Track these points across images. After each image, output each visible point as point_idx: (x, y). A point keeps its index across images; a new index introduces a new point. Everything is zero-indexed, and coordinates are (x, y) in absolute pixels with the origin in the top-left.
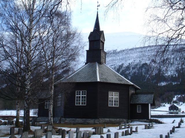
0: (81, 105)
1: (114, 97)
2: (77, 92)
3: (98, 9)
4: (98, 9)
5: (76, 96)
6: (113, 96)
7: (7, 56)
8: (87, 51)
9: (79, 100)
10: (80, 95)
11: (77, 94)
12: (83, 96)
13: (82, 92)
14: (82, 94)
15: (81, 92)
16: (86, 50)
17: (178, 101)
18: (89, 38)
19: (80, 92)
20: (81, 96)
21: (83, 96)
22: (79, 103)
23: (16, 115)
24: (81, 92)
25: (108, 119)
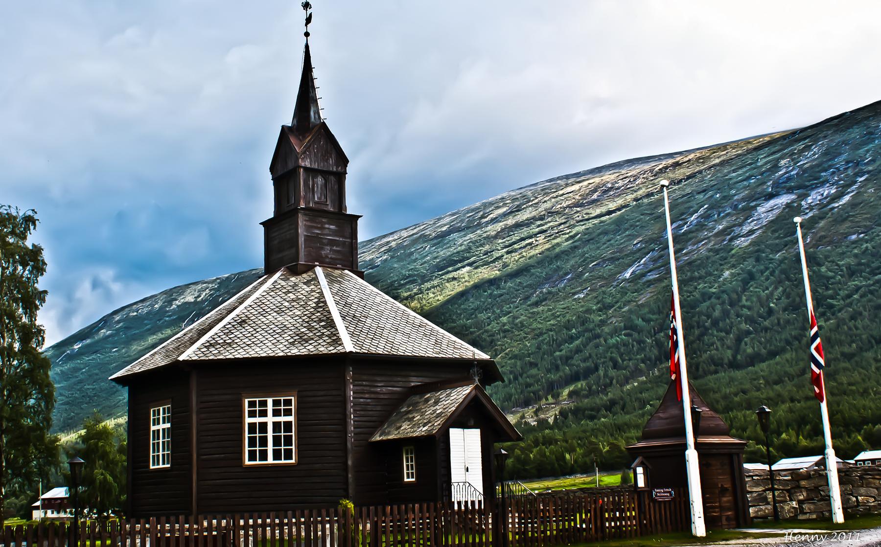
0: (270, 460)
1: (269, 423)
2: (252, 404)
3: (307, 34)
4: (307, 34)
5: (248, 420)
6: (274, 415)
7: (834, 289)
8: (266, 224)
9: (264, 442)
10: (266, 416)
11: (252, 414)
12: (277, 419)
13: (276, 403)
14: (276, 413)
15: (270, 401)
16: (357, 217)
17: (865, 433)
18: (272, 169)
19: (264, 404)
20: (270, 419)
21: (277, 419)
22: (264, 455)
23: (704, 535)
24: (270, 401)
25: (242, 539)
